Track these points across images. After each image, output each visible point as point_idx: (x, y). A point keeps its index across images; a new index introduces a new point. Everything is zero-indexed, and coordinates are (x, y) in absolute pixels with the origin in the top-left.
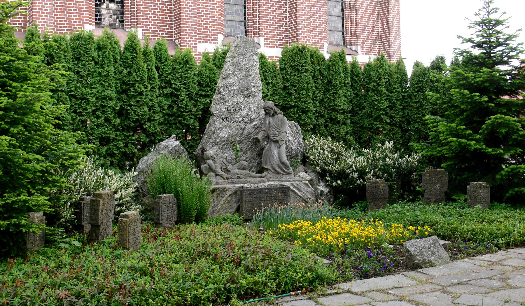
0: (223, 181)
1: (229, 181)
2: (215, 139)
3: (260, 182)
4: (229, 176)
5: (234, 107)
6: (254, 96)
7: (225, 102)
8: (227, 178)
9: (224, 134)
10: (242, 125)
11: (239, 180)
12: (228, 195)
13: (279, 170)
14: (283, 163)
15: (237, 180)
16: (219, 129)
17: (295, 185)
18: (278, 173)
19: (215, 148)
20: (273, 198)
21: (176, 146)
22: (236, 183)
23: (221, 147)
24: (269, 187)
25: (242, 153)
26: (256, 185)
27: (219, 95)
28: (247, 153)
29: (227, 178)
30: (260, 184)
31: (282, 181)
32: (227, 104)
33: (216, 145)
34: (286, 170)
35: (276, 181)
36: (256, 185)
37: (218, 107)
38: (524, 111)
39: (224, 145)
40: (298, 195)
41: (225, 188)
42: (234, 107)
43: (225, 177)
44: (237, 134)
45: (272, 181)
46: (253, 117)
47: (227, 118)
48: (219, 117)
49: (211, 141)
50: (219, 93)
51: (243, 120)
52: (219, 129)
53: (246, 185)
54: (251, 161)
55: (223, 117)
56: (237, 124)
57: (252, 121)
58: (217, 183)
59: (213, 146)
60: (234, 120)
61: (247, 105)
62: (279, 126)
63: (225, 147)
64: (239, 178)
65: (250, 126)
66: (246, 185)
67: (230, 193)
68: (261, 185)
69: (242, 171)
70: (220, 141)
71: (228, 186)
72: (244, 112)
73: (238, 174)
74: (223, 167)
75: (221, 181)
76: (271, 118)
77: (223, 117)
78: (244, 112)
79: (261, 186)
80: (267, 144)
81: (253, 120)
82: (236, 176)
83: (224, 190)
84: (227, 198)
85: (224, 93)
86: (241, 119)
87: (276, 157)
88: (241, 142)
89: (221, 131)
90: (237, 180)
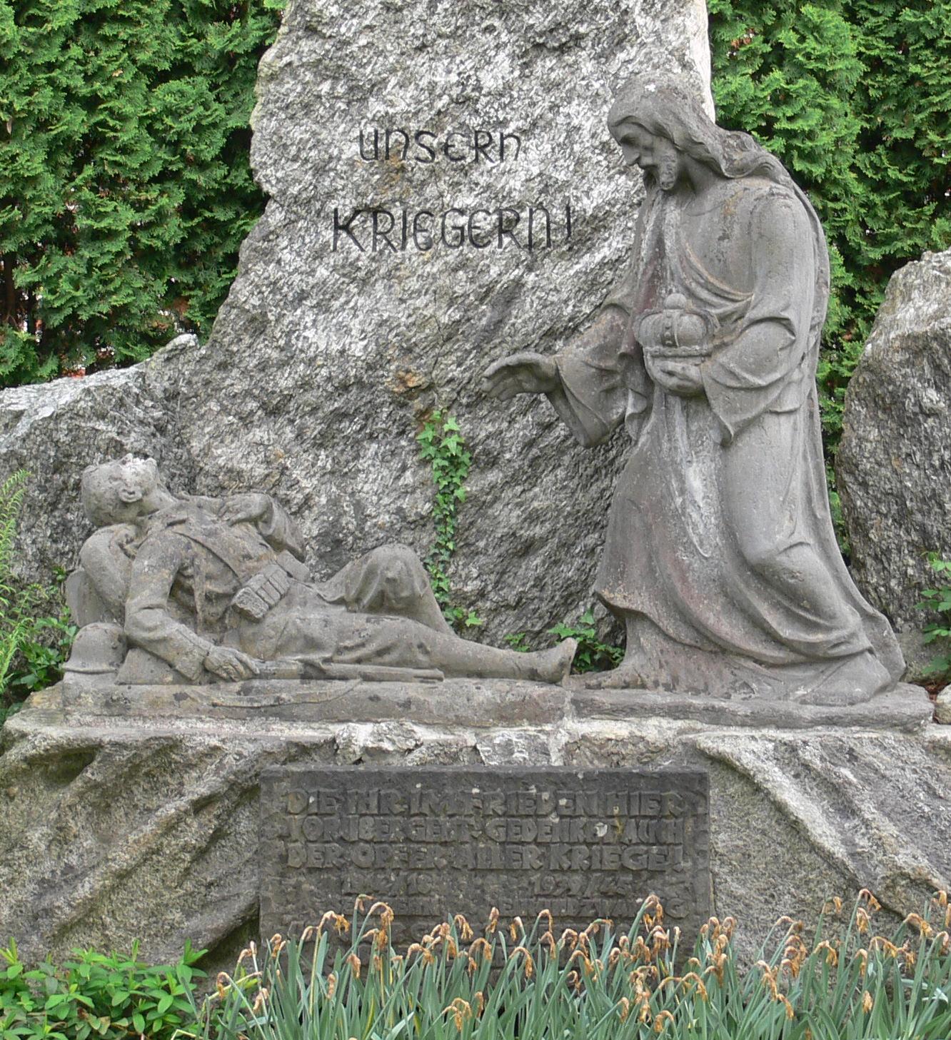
0: (166, 691)
1: (226, 695)
2: (263, 366)
3: (506, 714)
4: (224, 654)
5: (435, 126)
6: (620, 43)
7: (360, 94)
8: (210, 675)
9: (334, 337)
10: (498, 262)
11: (315, 688)
12: (182, 803)
13: (729, 629)
14: (765, 575)
15: (290, 690)
16: (302, 297)
17: (811, 755)
18: (720, 649)
19: (258, 434)
20: (531, 856)
21: (56, 418)
22: (279, 711)
23: (314, 427)
24: (586, 763)
25: (494, 476)
26: (470, 738)
27: (306, 45)
28: (533, 479)
29: (210, 675)
30: (501, 734)
31: (717, 717)
32: (376, 107)
33: (273, 412)
34: (787, 631)
35: (652, 711)
36: (470, 738)
37: (298, 133)
38: (326, 6)
39: (341, 415)
40: (815, 848)
41: (172, 744)
42: (435, 126)
43: (187, 664)
44: (450, 334)
45: (615, 712)
46: (588, 205)
47: (375, 212)
48: (307, 205)
49: (235, 382)
50: (311, 31)
51: (504, 228)
52: (302, 297)
53: (362, 734)
54: (566, 546)
55: (344, 205)
56: (452, 257)
57: (579, 233)
58: (114, 706)
59: (246, 420)
60: (432, 227)
61: (554, 107)
62: (724, 275)
63: (350, 428)
64: (312, 673)
65: (561, 275)
66: (362, 734)
67: (198, 788)
68: (507, 745)
69: (359, 620)
70: (305, 385)
71: (200, 731)
72: (520, 170)
73: (312, 644)
74: (202, 587)
75: (154, 689)
76: (673, 213)
77: (344, 205)
78: (520, 170)
79: (508, 747)
80: (644, 415)
81: (600, 222)
82: (292, 662)
83: (163, 759)
84: (170, 827)
85: (346, 29)
86: (485, 222)
87: (702, 517)
88: (476, 400)
89: (323, 307)
90: (290, 690)
